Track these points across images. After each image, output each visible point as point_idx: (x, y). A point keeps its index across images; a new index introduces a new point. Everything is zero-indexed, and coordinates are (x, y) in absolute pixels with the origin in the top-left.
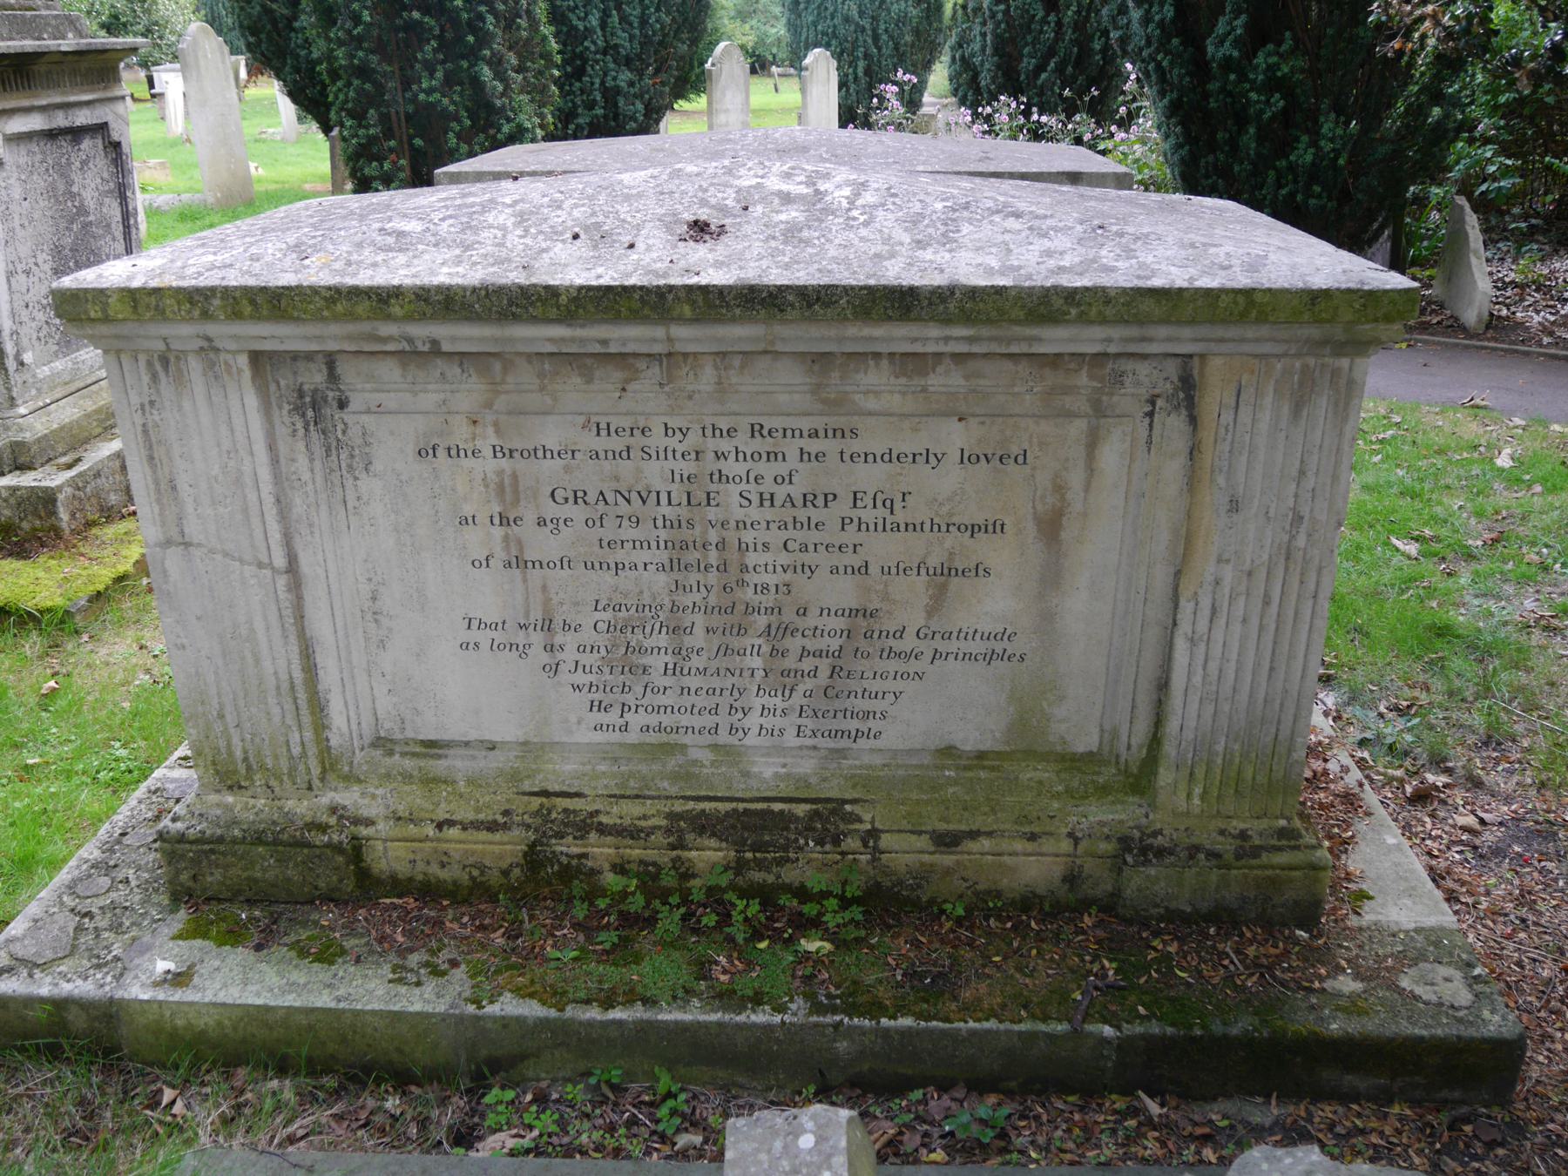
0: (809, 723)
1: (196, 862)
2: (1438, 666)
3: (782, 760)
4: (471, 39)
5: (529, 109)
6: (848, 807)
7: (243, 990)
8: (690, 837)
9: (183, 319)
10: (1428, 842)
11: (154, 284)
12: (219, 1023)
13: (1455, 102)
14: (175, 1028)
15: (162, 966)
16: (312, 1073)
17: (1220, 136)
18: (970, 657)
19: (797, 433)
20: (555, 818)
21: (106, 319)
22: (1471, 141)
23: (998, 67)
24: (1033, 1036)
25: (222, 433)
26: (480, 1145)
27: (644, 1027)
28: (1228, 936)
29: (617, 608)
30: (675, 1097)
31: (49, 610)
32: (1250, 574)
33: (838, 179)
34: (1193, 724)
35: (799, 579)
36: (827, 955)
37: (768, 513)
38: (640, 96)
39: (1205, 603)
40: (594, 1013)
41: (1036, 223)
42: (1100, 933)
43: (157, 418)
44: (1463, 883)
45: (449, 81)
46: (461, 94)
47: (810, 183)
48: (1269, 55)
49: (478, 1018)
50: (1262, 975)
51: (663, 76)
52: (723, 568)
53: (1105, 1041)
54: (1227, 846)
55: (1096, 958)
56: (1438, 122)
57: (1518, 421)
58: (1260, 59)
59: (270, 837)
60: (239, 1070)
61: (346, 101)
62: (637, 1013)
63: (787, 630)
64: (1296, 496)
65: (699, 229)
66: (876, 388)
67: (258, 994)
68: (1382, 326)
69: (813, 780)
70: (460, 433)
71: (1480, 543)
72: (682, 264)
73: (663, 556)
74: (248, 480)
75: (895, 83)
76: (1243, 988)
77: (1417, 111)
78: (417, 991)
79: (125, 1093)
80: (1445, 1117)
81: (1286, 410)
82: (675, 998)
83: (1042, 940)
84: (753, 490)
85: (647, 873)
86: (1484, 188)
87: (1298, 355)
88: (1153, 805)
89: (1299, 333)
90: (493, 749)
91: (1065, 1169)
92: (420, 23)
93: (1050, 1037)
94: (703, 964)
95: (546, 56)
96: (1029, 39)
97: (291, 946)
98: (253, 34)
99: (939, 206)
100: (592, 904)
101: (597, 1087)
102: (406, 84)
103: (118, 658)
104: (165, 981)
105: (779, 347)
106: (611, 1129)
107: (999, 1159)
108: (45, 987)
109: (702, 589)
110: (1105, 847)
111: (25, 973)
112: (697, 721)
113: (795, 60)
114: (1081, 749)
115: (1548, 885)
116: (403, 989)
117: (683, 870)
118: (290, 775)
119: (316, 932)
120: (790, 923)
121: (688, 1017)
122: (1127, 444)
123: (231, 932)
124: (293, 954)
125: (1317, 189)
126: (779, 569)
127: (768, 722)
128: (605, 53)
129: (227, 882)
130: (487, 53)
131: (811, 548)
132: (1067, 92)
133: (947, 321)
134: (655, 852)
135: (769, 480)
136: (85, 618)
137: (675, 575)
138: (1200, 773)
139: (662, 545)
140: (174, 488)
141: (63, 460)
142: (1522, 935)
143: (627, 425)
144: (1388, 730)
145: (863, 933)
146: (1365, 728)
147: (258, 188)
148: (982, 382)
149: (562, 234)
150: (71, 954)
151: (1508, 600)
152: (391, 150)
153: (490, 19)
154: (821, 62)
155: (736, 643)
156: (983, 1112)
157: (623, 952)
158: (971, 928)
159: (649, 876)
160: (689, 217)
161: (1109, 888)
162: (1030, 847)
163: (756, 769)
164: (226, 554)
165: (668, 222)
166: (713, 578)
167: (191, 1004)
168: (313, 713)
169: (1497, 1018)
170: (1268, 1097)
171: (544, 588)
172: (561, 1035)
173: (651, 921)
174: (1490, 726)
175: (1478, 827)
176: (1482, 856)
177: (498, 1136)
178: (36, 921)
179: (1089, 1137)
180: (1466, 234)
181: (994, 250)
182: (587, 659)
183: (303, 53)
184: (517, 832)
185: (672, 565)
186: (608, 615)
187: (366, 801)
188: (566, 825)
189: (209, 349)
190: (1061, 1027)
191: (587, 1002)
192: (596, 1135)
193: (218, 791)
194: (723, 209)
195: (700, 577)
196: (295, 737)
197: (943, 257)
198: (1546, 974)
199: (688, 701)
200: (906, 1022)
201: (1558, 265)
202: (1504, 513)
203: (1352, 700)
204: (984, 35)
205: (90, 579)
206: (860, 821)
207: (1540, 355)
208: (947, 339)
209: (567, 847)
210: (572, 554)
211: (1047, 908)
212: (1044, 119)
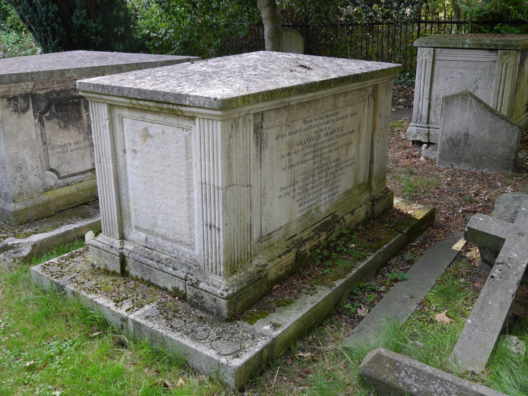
193: (231, 276)
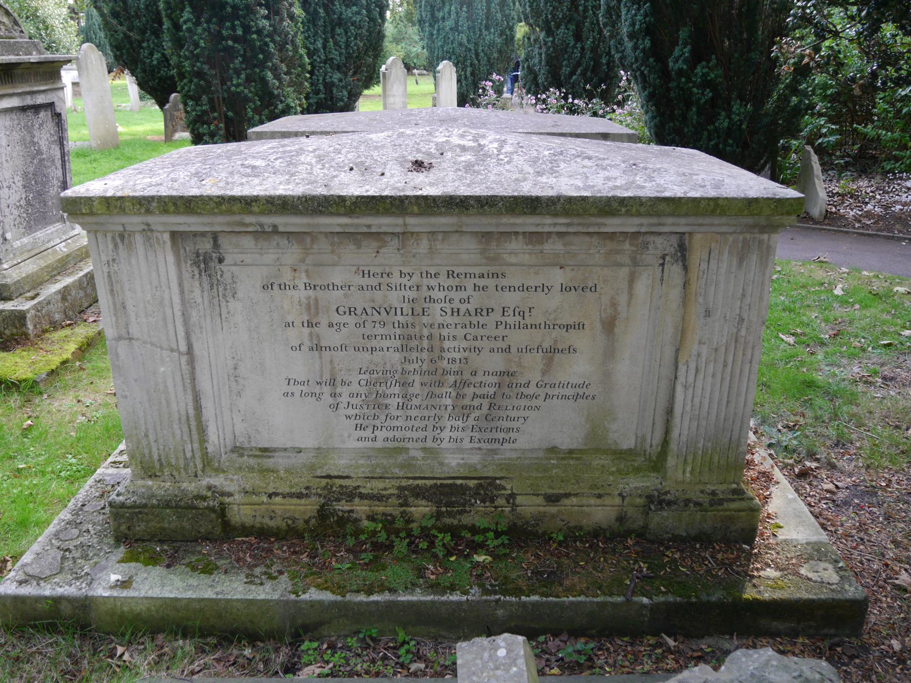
0: (477, 435)
1: (130, 519)
2: (809, 403)
3: (461, 456)
4: (261, 56)
5: (293, 96)
6: (498, 482)
7: (162, 590)
8: (411, 500)
9: (135, 214)
10: (808, 498)
11: (119, 194)
12: (149, 609)
13: (804, 94)
14: (123, 612)
15: (114, 577)
16: (202, 636)
17: (676, 112)
18: (565, 397)
19: (472, 276)
20: (335, 489)
21: (92, 214)
22: (812, 115)
23: (549, 72)
24: (603, 605)
25: (152, 277)
26: (300, 673)
27: (390, 605)
28: (706, 549)
29: (372, 372)
30: (408, 643)
31: (25, 380)
32: (716, 350)
33: (490, 138)
34: (686, 432)
35: (473, 355)
36: (489, 563)
37: (456, 319)
38: (345, 87)
39: (693, 366)
40: (362, 598)
41: (600, 162)
42: (638, 549)
43: (116, 268)
44: (829, 520)
45: (248, 80)
46: (255, 87)
47: (475, 140)
48: (703, 68)
49: (296, 601)
50: (726, 569)
51: (358, 76)
52: (431, 349)
53: (644, 606)
54: (705, 499)
55: (636, 562)
56: (795, 105)
57: (844, 270)
58: (698, 70)
59: (174, 504)
60: (159, 636)
61: (189, 91)
62: (386, 597)
63: (466, 384)
64: (741, 308)
65: (418, 165)
66: (516, 251)
67: (171, 592)
68: (785, 217)
69: (479, 467)
70: (287, 276)
71: (827, 336)
72: (412, 184)
73: (398, 343)
74: (167, 302)
75: (490, 81)
76: (717, 576)
77: (784, 99)
78: (261, 588)
79: (95, 650)
80: (827, 643)
81: (735, 262)
82: (406, 588)
83: (606, 553)
84: (448, 307)
85: (387, 520)
86: (820, 141)
87: (740, 233)
88: (664, 478)
89: (742, 220)
90: (300, 452)
91: (625, 676)
92: (233, 47)
93: (614, 605)
94: (420, 570)
95: (302, 66)
96: (566, 56)
97: (187, 565)
98: (118, 50)
99: (546, 153)
100: (356, 538)
101: (364, 639)
102: (223, 82)
103: (63, 408)
104: (116, 585)
105: (464, 229)
106: (373, 661)
107: (589, 672)
108: (47, 591)
109: (419, 361)
110: (640, 501)
111: (35, 583)
112: (415, 435)
113: (431, 67)
114: (625, 447)
115: (874, 520)
116: (253, 587)
117: (407, 518)
118: (185, 469)
119: (200, 557)
120: (467, 546)
121: (415, 598)
122: (650, 281)
123: (151, 558)
124: (188, 569)
125: (731, 141)
126: (462, 350)
127: (454, 435)
128: (325, 62)
129: (146, 529)
130: (270, 64)
131: (479, 338)
132: (588, 87)
133: (556, 215)
134: (392, 508)
135: (457, 301)
136: (45, 385)
137: (404, 354)
138: (690, 460)
139: (397, 337)
140: (124, 308)
141: (28, 295)
142: (862, 547)
143: (379, 272)
144: (784, 439)
145: (508, 551)
146: (771, 438)
147: (121, 138)
148: (573, 247)
149: (343, 167)
150: (60, 572)
151: (844, 367)
152: (215, 118)
153: (271, 45)
154: (447, 69)
155: (437, 391)
156: (579, 646)
157: (375, 564)
158: (567, 547)
159: (388, 522)
160: (411, 158)
161: (641, 524)
162: (598, 501)
163: (447, 461)
164: (152, 344)
165: (401, 161)
166: (425, 355)
167: (133, 598)
168: (199, 434)
169: (852, 589)
170: (732, 635)
171: (331, 361)
172: (343, 610)
173: (390, 547)
174: (838, 435)
175: (835, 490)
176: (837, 505)
177: (310, 667)
178: (38, 554)
179: (637, 660)
180: (812, 167)
181: (579, 177)
182: (354, 401)
183: (148, 61)
184: (314, 499)
185: (403, 348)
186: (366, 376)
187: (228, 483)
188: (341, 494)
189: (148, 230)
190: (620, 599)
191: (358, 591)
192: (365, 666)
193: (143, 479)
194: (429, 154)
195: (418, 355)
196: (188, 447)
197: (552, 180)
198: (875, 567)
199: (410, 423)
200: (535, 598)
201: (861, 184)
202: (840, 320)
203: (763, 422)
204: (540, 54)
205: (48, 362)
206: (505, 489)
207: (854, 233)
208: (555, 225)
209: (342, 506)
210: (347, 342)
211: (608, 535)
212: (576, 101)
